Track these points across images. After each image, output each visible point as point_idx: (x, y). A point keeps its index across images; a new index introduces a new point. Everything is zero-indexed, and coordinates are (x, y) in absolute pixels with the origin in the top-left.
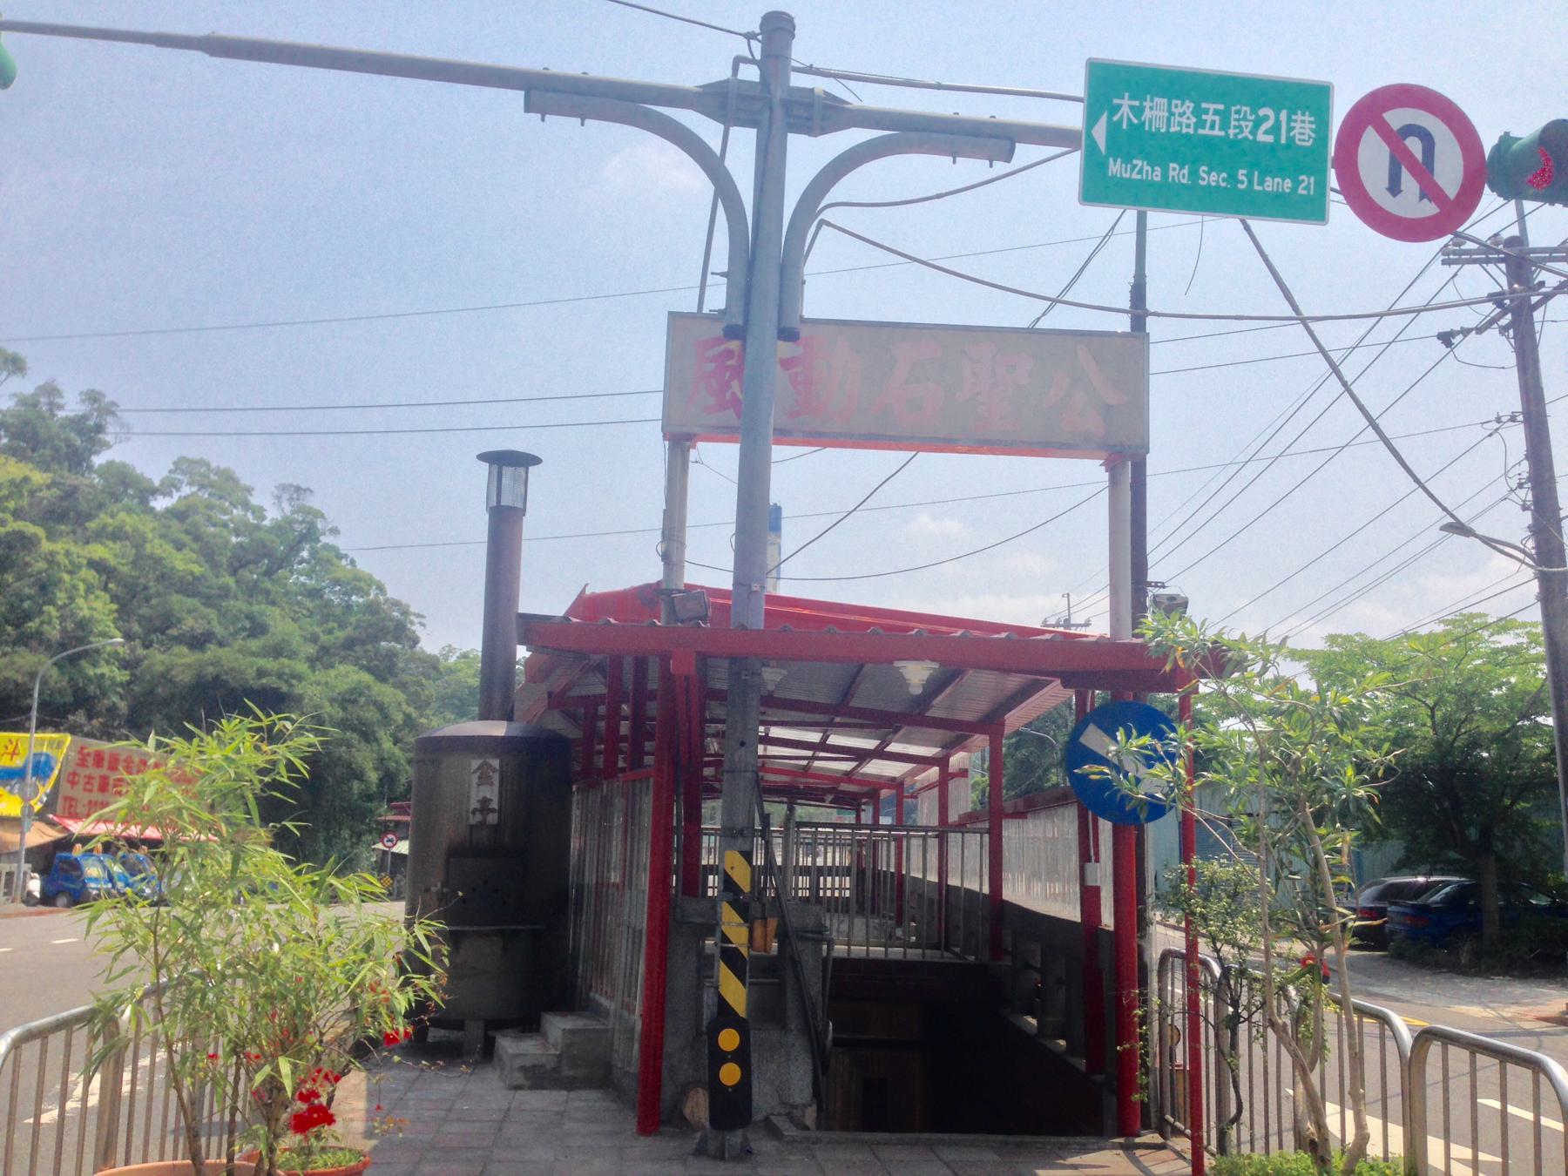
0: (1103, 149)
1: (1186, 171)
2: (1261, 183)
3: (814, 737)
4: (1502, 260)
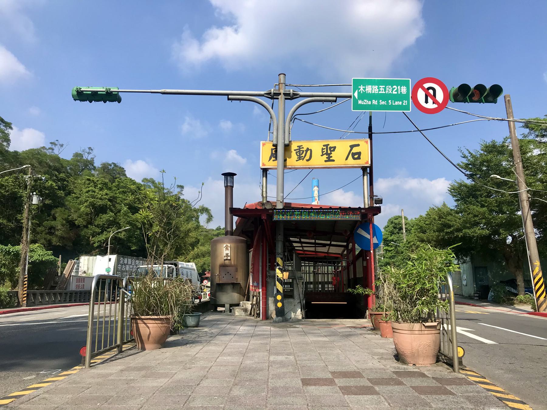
3: (313, 241)
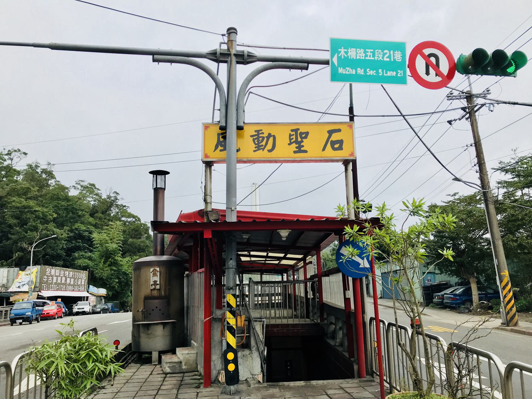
0: (336, 64)
1: (363, 70)
2: (386, 73)
3: (265, 254)
4: (465, 98)
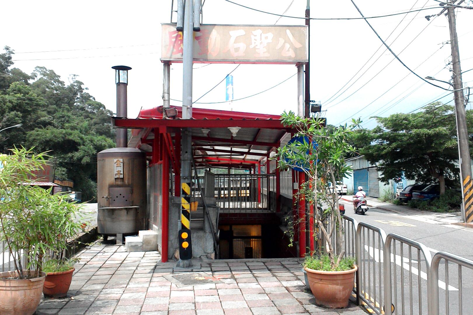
3: (228, 149)
